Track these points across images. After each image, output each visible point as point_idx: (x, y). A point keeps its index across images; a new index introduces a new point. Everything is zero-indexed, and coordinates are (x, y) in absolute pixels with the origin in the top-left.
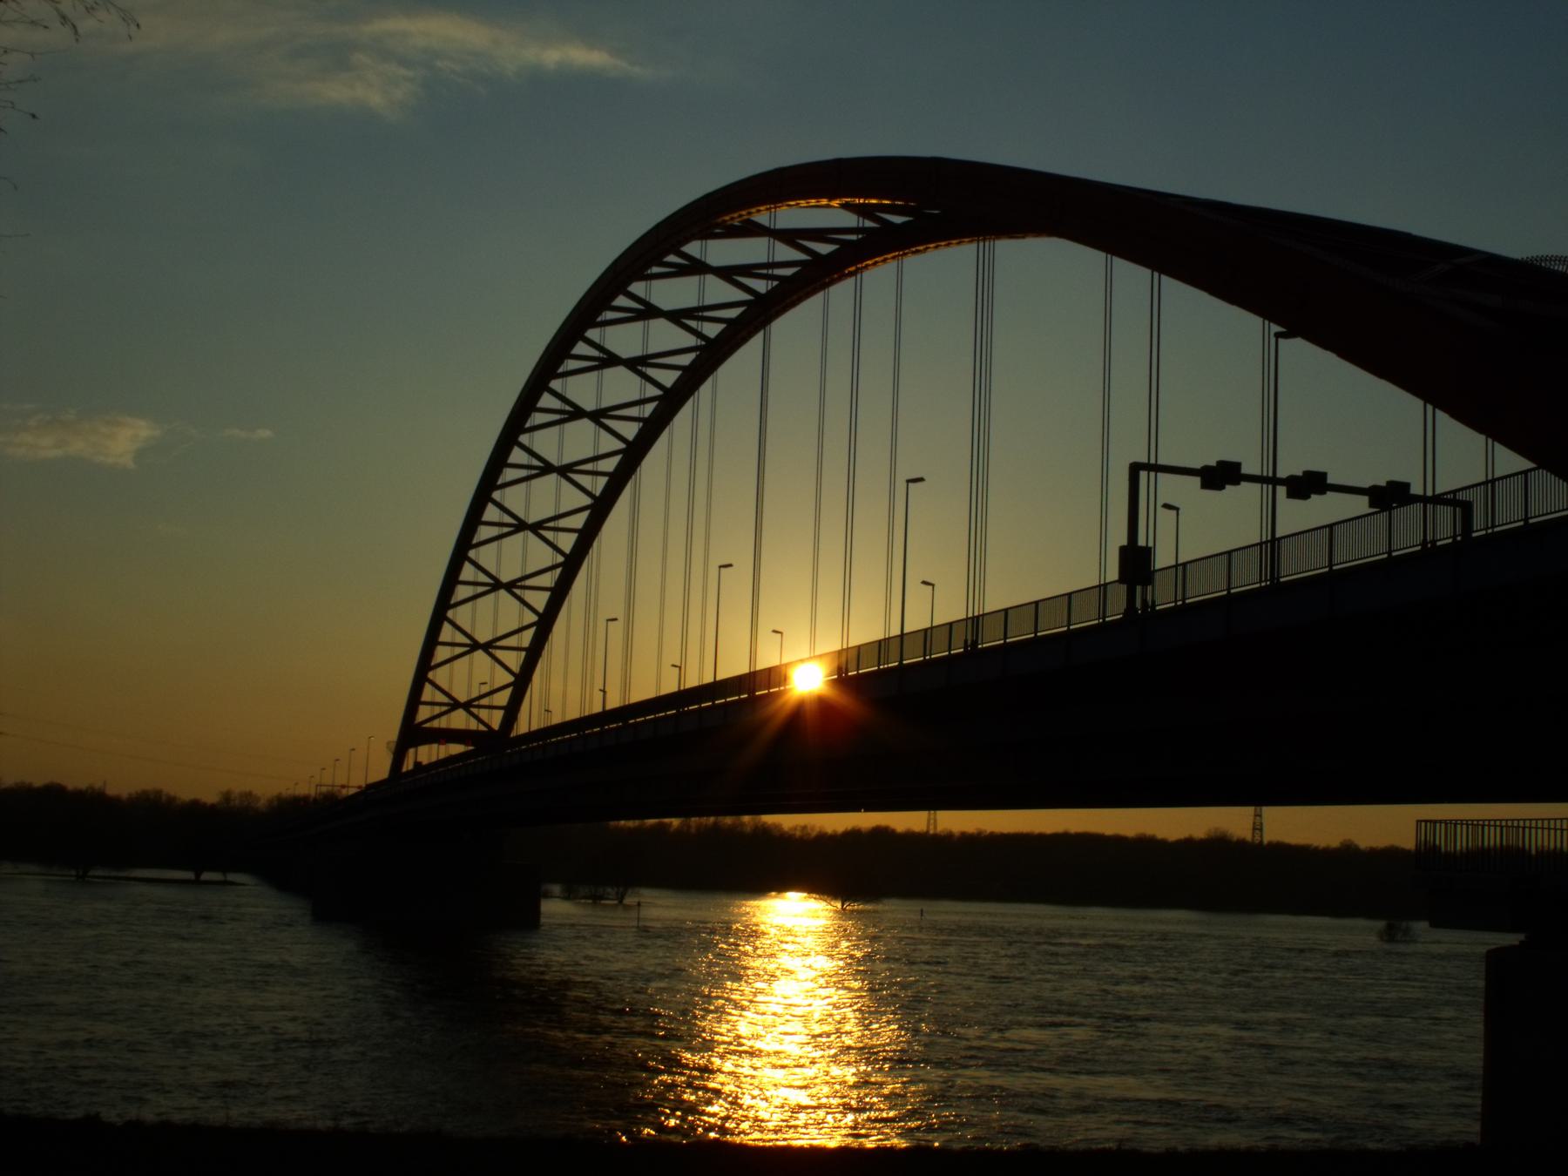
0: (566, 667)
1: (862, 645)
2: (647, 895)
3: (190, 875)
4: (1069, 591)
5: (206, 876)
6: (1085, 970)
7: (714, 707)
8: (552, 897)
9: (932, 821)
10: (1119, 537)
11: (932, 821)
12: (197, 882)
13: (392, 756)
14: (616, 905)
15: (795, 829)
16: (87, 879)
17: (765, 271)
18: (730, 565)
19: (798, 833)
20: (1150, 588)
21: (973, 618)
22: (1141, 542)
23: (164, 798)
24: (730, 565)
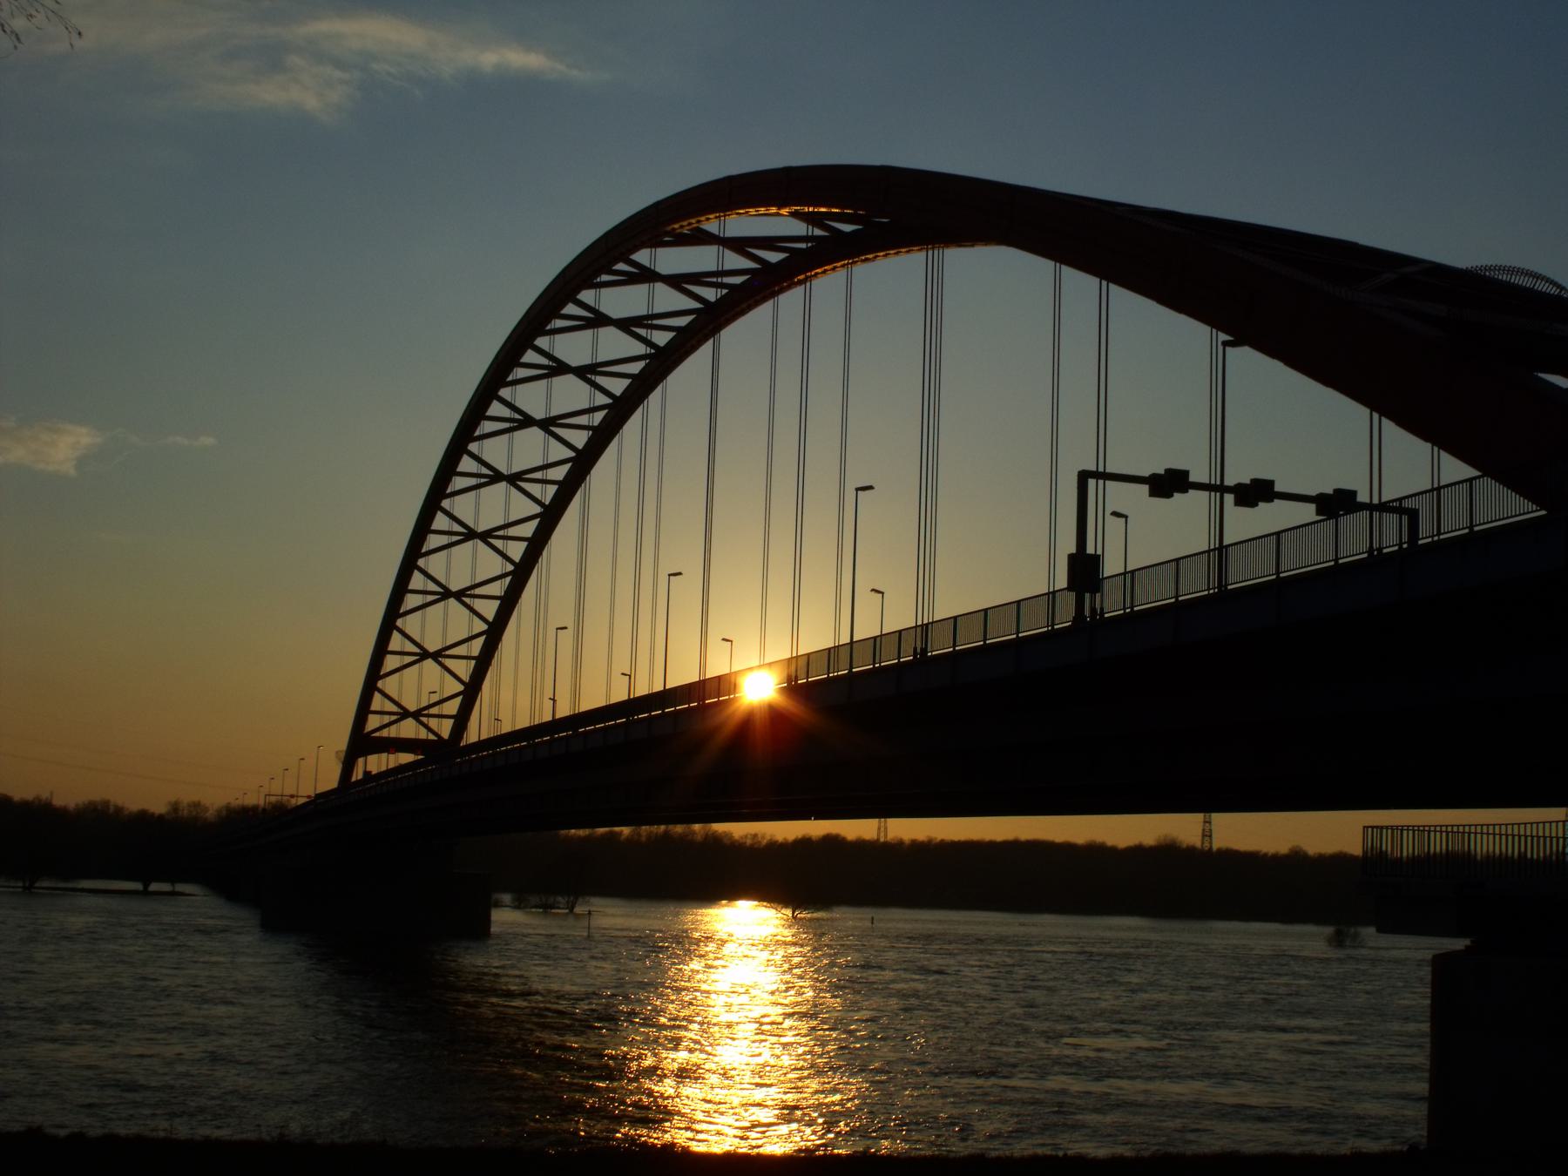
2: (597, 903)
3: (138, 886)
5: (154, 887)
8: (502, 906)
9: (882, 829)
11: (882, 829)
12: (145, 893)
13: (341, 765)
14: (567, 913)
15: (746, 836)
19: (749, 842)
21: (922, 625)
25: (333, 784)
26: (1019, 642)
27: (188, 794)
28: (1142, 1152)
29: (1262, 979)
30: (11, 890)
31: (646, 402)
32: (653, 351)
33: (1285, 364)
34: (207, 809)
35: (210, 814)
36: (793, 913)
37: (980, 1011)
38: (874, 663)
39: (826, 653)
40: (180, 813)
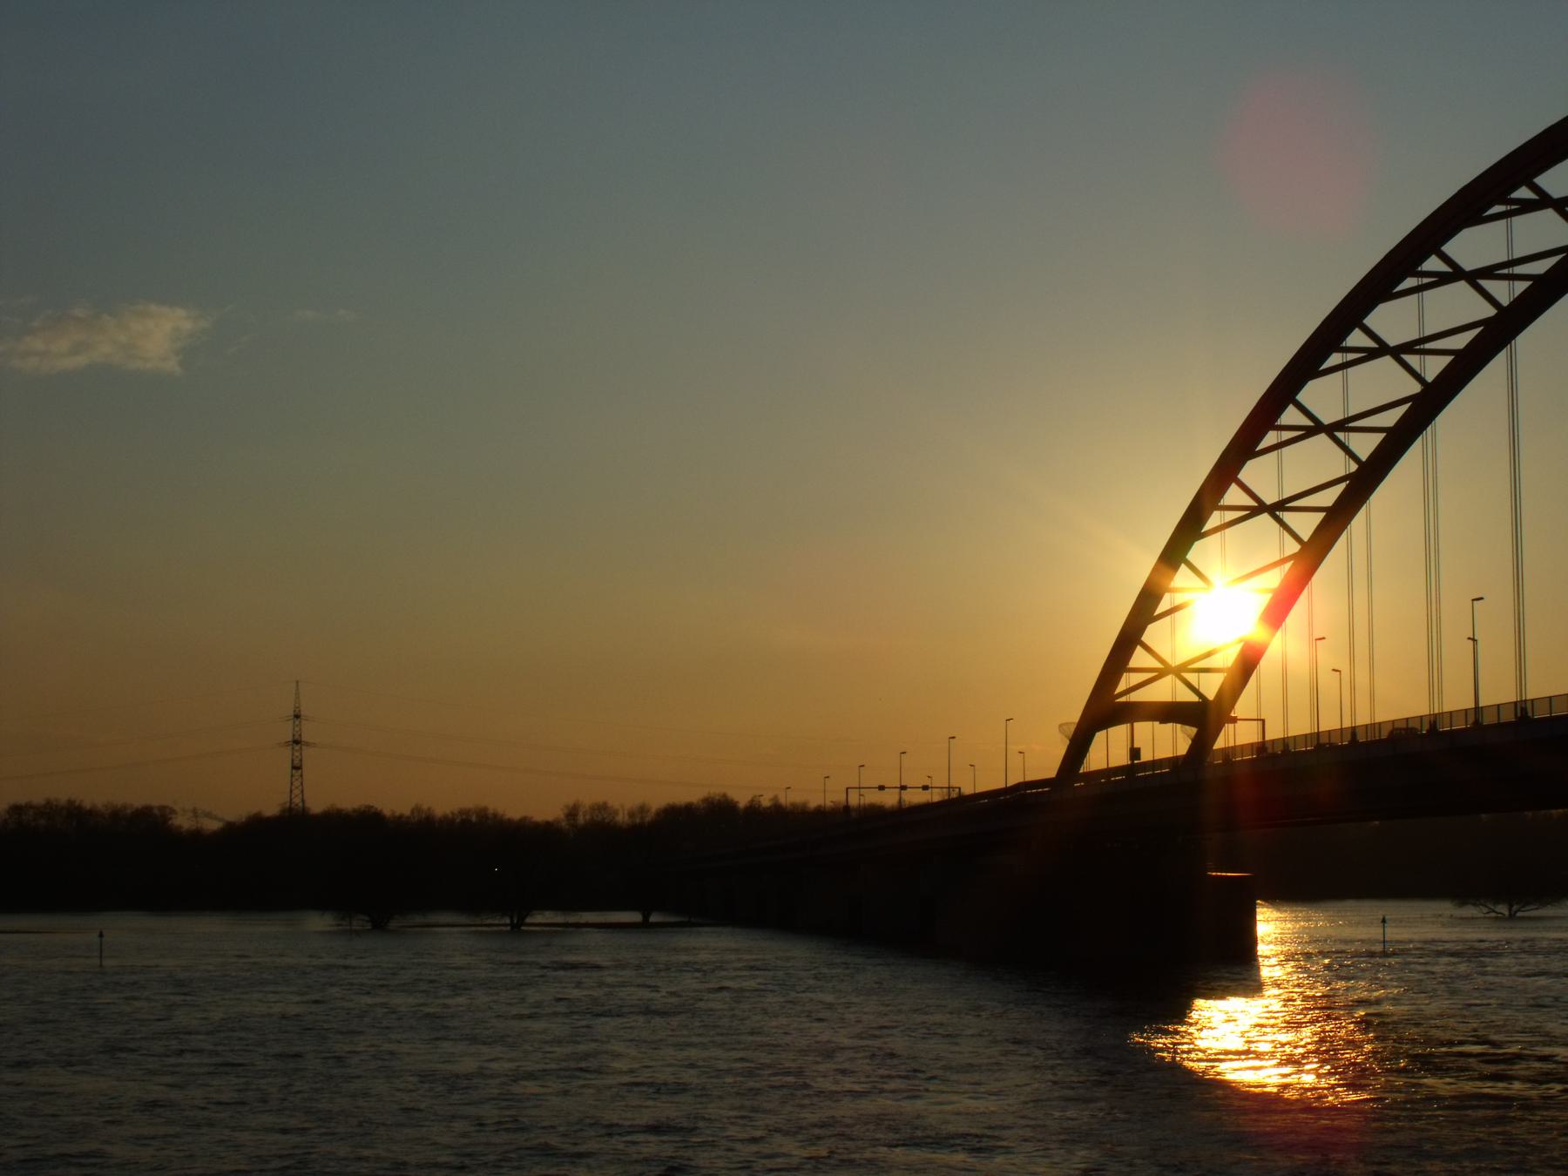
0: (17, 932)
1: (1384, 722)
3: (635, 917)
4: (1552, 695)
5: (654, 918)
6: (1422, 918)
7: (1154, 775)
10: (909, 786)
12: (645, 925)
16: (523, 928)
17: (1505, 271)
18: (1482, 599)
20: (1519, 715)
21: (1521, 701)
22: (1135, 746)
23: (474, 818)
24: (1482, 599)
25: (1050, 771)
26: (1452, 731)
27: (589, 795)
28: (1222, 1067)
29: (238, 956)
30: (495, 928)
31: (1349, 527)
32: (1278, 513)
33: (75, 813)
34: (616, 813)
35: (622, 818)
36: (1510, 910)
37: (1448, 980)
38: (1467, 724)
39: (1513, 706)
40: (1270, 751)
